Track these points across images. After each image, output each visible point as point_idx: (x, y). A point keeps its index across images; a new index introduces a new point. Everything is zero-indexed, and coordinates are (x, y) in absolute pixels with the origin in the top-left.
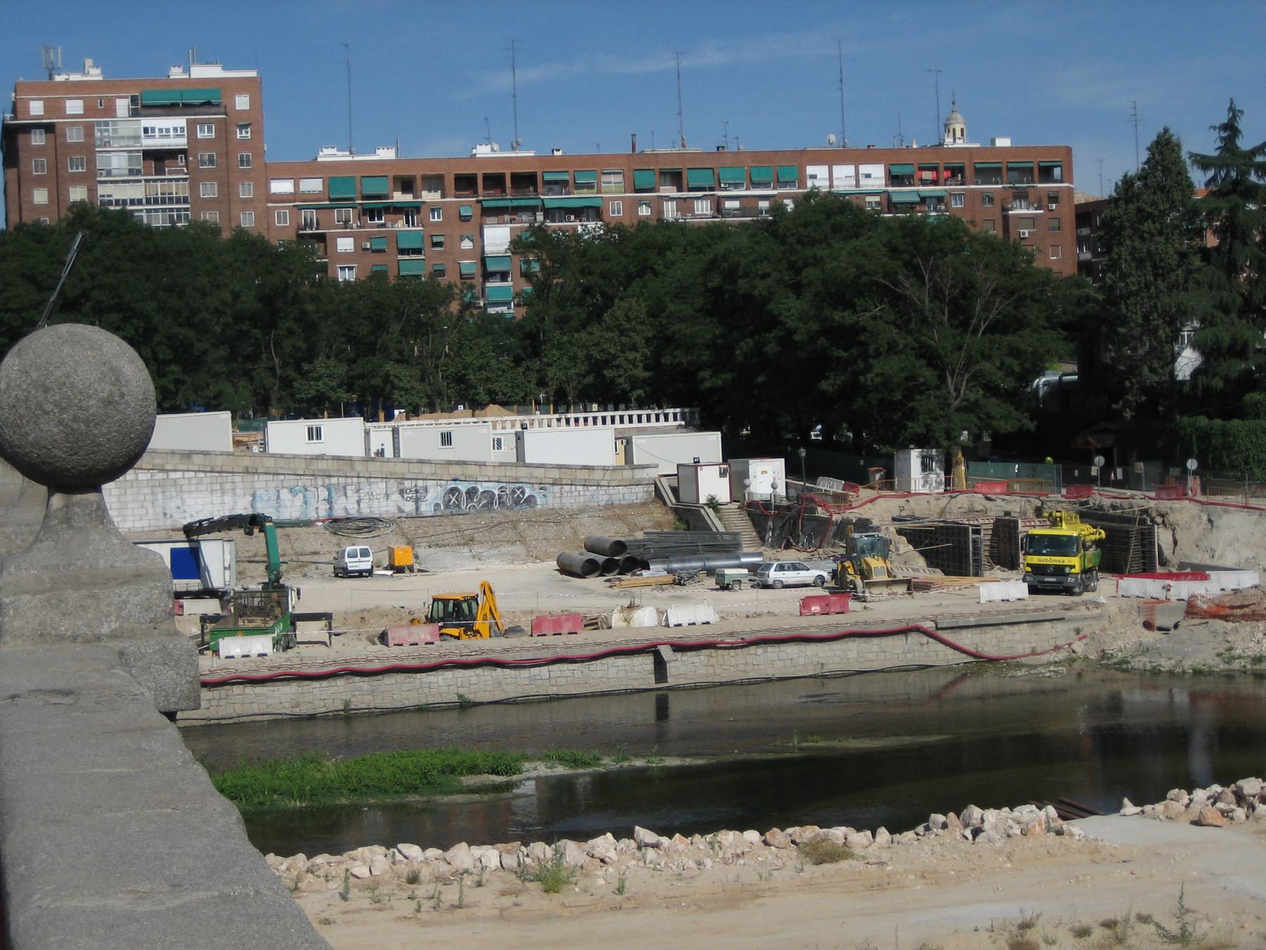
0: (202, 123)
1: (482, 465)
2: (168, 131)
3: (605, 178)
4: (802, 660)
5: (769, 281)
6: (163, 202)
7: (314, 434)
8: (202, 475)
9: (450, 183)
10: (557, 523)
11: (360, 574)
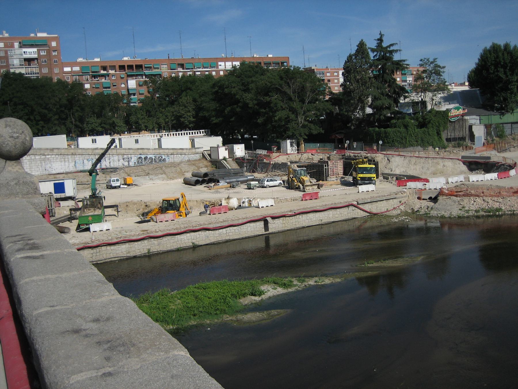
0: (42, 50)
1: (149, 149)
2: (31, 52)
3: (162, 66)
4: (314, 219)
5: (236, 89)
6: (31, 74)
7: (94, 141)
8: (57, 156)
9: (117, 67)
10: (175, 167)
11: (115, 188)
